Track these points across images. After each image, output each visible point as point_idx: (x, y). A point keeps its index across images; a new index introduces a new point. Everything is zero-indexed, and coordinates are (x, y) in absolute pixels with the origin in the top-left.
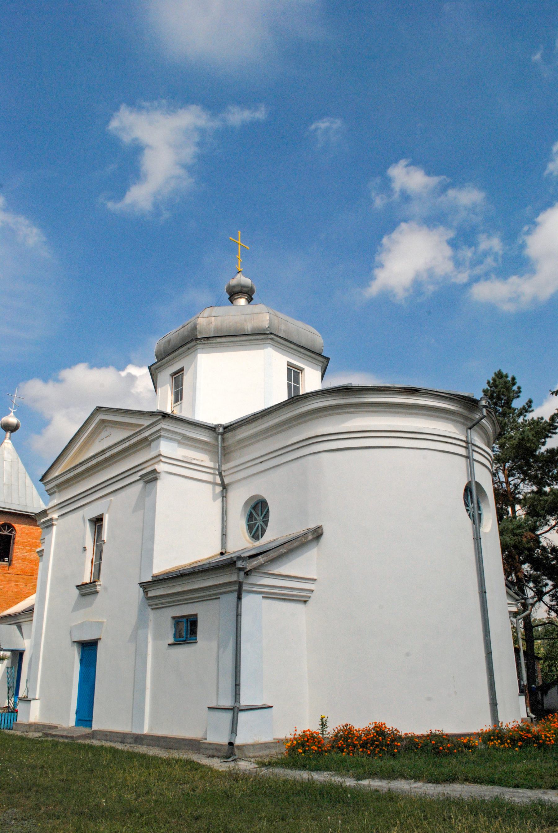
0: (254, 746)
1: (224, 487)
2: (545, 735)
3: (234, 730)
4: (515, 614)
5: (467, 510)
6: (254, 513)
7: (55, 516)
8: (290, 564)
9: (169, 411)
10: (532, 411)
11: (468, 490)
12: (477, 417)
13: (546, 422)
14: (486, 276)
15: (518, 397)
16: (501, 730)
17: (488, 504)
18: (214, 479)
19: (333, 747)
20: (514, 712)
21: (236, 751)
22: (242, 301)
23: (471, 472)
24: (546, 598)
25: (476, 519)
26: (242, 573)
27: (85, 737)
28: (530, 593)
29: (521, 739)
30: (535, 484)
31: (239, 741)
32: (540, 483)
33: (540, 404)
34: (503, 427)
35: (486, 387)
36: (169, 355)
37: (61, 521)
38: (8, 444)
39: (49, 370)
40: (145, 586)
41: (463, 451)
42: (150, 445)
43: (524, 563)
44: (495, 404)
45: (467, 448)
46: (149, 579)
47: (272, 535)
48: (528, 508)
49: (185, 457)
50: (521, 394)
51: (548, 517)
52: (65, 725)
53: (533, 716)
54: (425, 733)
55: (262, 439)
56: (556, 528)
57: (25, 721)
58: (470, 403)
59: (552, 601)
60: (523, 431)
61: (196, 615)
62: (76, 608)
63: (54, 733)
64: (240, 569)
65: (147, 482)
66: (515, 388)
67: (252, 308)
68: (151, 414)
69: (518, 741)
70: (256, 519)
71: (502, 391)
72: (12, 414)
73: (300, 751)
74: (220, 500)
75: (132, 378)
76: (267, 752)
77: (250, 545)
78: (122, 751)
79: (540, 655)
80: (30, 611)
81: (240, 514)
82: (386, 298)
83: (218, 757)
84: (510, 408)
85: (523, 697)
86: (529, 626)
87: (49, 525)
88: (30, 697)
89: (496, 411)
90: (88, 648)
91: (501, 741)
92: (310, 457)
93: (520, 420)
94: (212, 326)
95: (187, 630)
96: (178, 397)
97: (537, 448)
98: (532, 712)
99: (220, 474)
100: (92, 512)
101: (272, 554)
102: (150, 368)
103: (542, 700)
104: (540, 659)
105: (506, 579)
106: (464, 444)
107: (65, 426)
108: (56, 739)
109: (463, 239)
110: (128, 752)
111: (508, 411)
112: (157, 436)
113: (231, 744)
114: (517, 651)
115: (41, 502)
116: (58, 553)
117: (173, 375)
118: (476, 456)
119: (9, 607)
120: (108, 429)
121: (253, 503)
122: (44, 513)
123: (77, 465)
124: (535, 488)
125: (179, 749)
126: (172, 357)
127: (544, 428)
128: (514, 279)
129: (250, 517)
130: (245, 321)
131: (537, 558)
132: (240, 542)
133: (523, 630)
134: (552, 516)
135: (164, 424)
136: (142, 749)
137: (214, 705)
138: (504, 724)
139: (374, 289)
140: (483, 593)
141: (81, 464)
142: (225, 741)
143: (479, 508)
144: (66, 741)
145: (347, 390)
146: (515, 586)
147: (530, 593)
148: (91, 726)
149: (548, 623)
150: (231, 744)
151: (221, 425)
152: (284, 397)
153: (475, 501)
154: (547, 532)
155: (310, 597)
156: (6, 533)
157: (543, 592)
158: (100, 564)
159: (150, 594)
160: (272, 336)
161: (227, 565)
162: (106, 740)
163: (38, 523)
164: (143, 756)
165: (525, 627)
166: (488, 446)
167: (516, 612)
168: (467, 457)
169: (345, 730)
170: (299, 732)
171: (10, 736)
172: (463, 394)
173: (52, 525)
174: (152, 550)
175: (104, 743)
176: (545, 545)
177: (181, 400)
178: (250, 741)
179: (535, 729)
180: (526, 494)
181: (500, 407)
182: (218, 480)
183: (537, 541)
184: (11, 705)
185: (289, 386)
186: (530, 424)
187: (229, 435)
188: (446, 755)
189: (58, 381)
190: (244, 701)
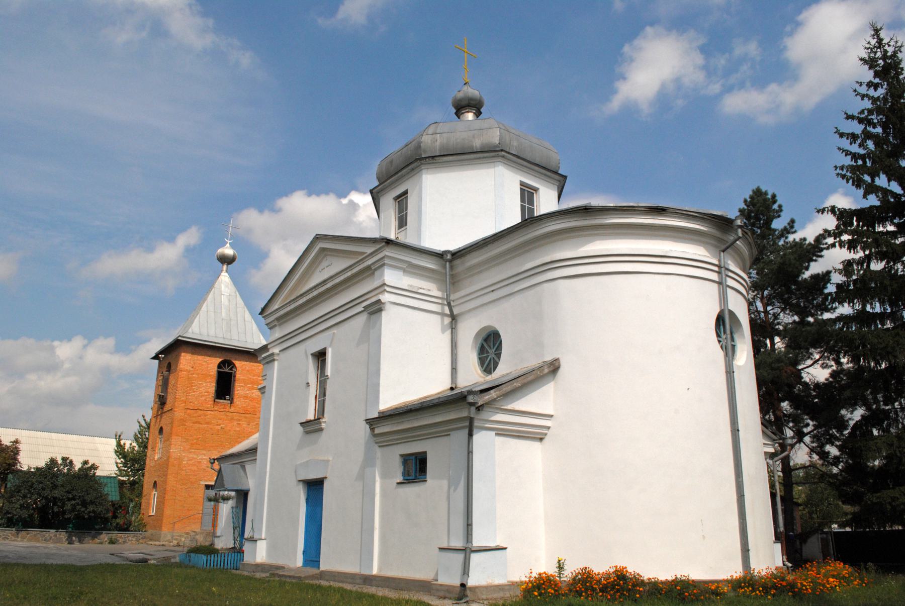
0: (488, 588)
1: (454, 318)
2: (801, 583)
3: (466, 571)
4: (772, 456)
5: (719, 341)
6: (485, 345)
7: (276, 350)
8: (524, 399)
9: (392, 237)
10: (795, 232)
11: (720, 320)
12: (732, 238)
13: (810, 244)
14: (742, 86)
15: (779, 216)
16: (752, 576)
17: (743, 335)
18: (443, 309)
19: (570, 590)
20: (768, 558)
21: (468, 593)
22: (470, 116)
23: (723, 299)
24: (807, 439)
25: (729, 351)
26: (473, 409)
27: (313, 577)
28: (789, 433)
29: (775, 587)
30: (796, 314)
31: (471, 582)
32: (803, 313)
33: (803, 227)
34: (761, 250)
35: (743, 206)
36: (392, 176)
37: (282, 355)
38: (225, 277)
39: (266, 200)
40: (372, 423)
41: (715, 276)
42: (373, 273)
43: (784, 401)
44: (753, 225)
45: (719, 273)
46: (376, 415)
47: (505, 369)
48: (790, 339)
49: (411, 286)
50: (782, 214)
51: (812, 350)
52: (292, 566)
53: (790, 565)
54: (670, 579)
55: (494, 266)
56: (820, 362)
57: (251, 561)
58: (722, 223)
59: (813, 442)
60: (784, 255)
61: (425, 453)
62: (300, 446)
63: (281, 573)
64: (472, 404)
65: (372, 313)
66: (775, 207)
67: (479, 123)
68: (374, 241)
69: (770, 589)
70: (488, 352)
71: (760, 208)
72: (228, 245)
73: (536, 594)
74: (449, 331)
75: (353, 206)
76: (501, 594)
77: (481, 380)
78: (351, 591)
79: (800, 501)
80: (253, 451)
81: (470, 347)
82: (630, 110)
83: (450, 599)
84: (770, 229)
85: (779, 545)
86: (787, 469)
87: (270, 360)
88: (256, 537)
89: (753, 232)
90: (314, 487)
91: (753, 589)
92: (546, 285)
93: (781, 243)
94: (438, 143)
95: (416, 468)
96: (402, 222)
97: (800, 272)
98: (788, 560)
99: (449, 304)
100: (315, 346)
101: (506, 389)
102: (371, 192)
103: (801, 549)
104: (798, 505)
105: (763, 418)
106: (716, 269)
107: (283, 259)
108: (283, 579)
109: (714, 43)
110: (357, 592)
111: (767, 232)
112: (381, 265)
113: (463, 585)
114: (773, 495)
115: (262, 337)
116: (281, 391)
117: (396, 198)
118: (730, 282)
119: (232, 446)
120: (329, 258)
121: (484, 335)
122: (265, 348)
123: (297, 297)
124: (796, 318)
125: (409, 590)
126: (394, 179)
127: (808, 251)
128: (773, 87)
129: (482, 351)
130: (474, 137)
131: (798, 395)
132: (471, 375)
133: (781, 474)
134: (815, 348)
135: (388, 252)
136: (372, 590)
137: (445, 545)
138: (756, 571)
139: (616, 103)
140: (735, 431)
141: (302, 295)
142: (457, 582)
143: (733, 339)
144: (294, 581)
145: (586, 210)
146: (773, 424)
147: (789, 433)
148: (319, 568)
149: (809, 466)
150: (463, 585)
151: (448, 252)
152: (518, 219)
153: (728, 332)
154: (810, 366)
155: (546, 434)
156: (227, 370)
157: (803, 432)
158: (324, 401)
159: (377, 431)
160: (503, 153)
161: (457, 399)
162: (334, 581)
163: (259, 359)
164: (373, 596)
165: (783, 471)
166: (744, 271)
167: (772, 453)
168: (720, 283)
169: (584, 574)
170: (534, 575)
171: (236, 575)
172: (715, 213)
173: (274, 360)
174: (378, 384)
175: (332, 583)
176: (808, 380)
177: (406, 224)
178: (483, 583)
179: (790, 578)
180: (787, 324)
181: (758, 228)
182: (447, 311)
183: (798, 375)
184: (237, 546)
185: (523, 208)
186: (791, 247)
187: (457, 262)
188: (692, 601)
189: (276, 211)
190: (477, 542)
